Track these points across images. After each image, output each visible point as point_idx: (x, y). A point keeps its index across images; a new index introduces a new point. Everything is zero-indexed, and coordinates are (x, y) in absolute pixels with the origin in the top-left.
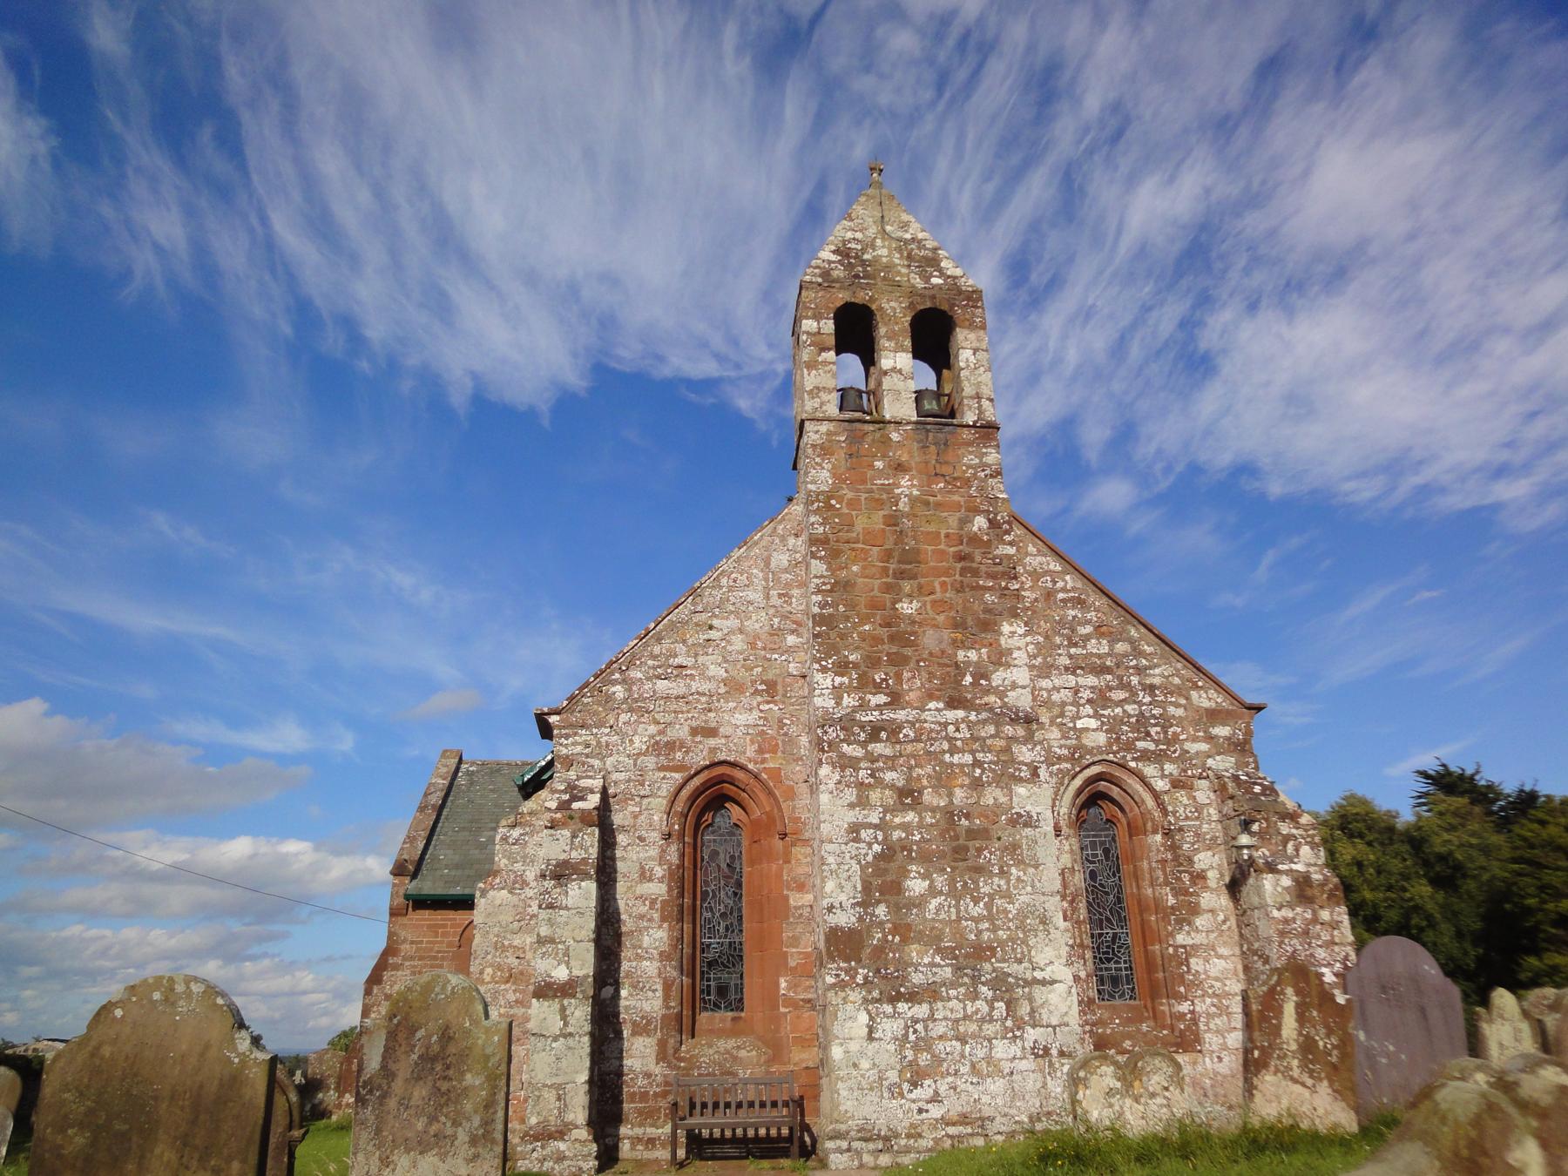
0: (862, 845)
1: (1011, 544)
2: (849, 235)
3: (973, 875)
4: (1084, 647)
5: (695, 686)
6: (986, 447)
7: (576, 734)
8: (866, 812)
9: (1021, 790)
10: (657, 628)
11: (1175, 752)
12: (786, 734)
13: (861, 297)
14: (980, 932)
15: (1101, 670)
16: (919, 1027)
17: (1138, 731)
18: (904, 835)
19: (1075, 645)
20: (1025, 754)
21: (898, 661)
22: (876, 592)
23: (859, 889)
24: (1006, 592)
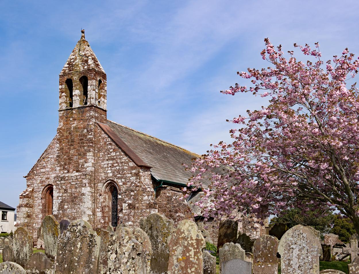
4: (111, 155)
6: (91, 111)
9: (83, 188)
11: (124, 176)
14: (75, 215)
15: (113, 159)
17: (118, 172)
19: (109, 154)
21: (70, 163)
22: (67, 150)
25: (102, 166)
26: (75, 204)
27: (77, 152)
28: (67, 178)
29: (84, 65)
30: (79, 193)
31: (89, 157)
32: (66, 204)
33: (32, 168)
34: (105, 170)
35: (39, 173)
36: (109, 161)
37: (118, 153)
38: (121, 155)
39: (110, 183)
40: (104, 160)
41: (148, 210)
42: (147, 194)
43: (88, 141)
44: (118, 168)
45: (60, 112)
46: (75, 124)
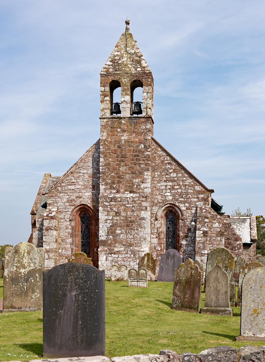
1: (149, 152)
4: (170, 175)
5: (77, 187)
6: (147, 123)
7: (51, 198)
8: (108, 217)
9: (143, 212)
10: (68, 173)
11: (188, 201)
13: (116, 78)
16: (116, 259)
17: (180, 196)
18: (116, 222)
19: (168, 175)
20: (144, 204)
21: (119, 182)
22: (115, 166)
23: (107, 232)
24: (147, 164)
25: (158, 187)
26: (132, 229)
27: (130, 170)
28: (119, 200)
29: (137, 66)
30: (137, 217)
31: (147, 177)
36: (168, 183)
37: (180, 175)
38: (185, 177)
39: (169, 207)
40: (161, 180)
41: (219, 238)
42: (218, 222)
43: (146, 158)
44: (179, 191)
45: (102, 120)
46: (125, 137)
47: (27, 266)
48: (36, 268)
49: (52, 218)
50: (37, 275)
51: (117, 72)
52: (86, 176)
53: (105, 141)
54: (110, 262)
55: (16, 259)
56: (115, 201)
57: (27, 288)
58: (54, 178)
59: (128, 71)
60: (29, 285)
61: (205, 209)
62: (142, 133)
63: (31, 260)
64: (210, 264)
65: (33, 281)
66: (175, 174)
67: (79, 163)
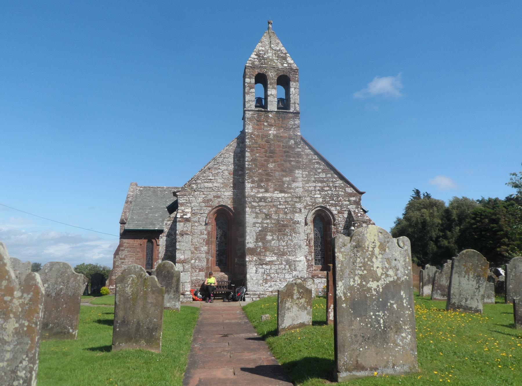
0: (256, 228)
1: (300, 148)
2: (261, 48)
3: (283, 236)
5: (215, 184)
6: (296, 119)
7: (183, 197)
9: (297, 215)
11: (340, 204)
12: (238, 198)
13: (263, 71)
15: (322, 182)
16: (268, 271)
17: (331, 198)
19: (316, 175)
20: (298, 205)
21: (268, 180)
22: (263, 162)
23: (255, 238)
24: (298, 162)
26: (285, 235)
27: (279, 167)
32: (269, 234)
33: (190, 181)
34: (311, 194)
35: (201, 188)
36: (317, 183)
37: (329, 175)
46: (272, 132)
47: (382, 274)
48: (398, 279)
49: (188, 220)
50: (402, 294)
51: (263, 66)
52: (226, 173)
53: (251, 134)
54: (261, 275)
55: (358, 260)
56: (265, 202)
57: (384, 322)
58: (141, 187)
59: (274, 65)
60: (389, 316)
61: (359, 213)
62: (291, 128)
63: (389, 263)
64: (457, 272)
65: (395, 306)
66: (324, 174)
67: (218, 157)
